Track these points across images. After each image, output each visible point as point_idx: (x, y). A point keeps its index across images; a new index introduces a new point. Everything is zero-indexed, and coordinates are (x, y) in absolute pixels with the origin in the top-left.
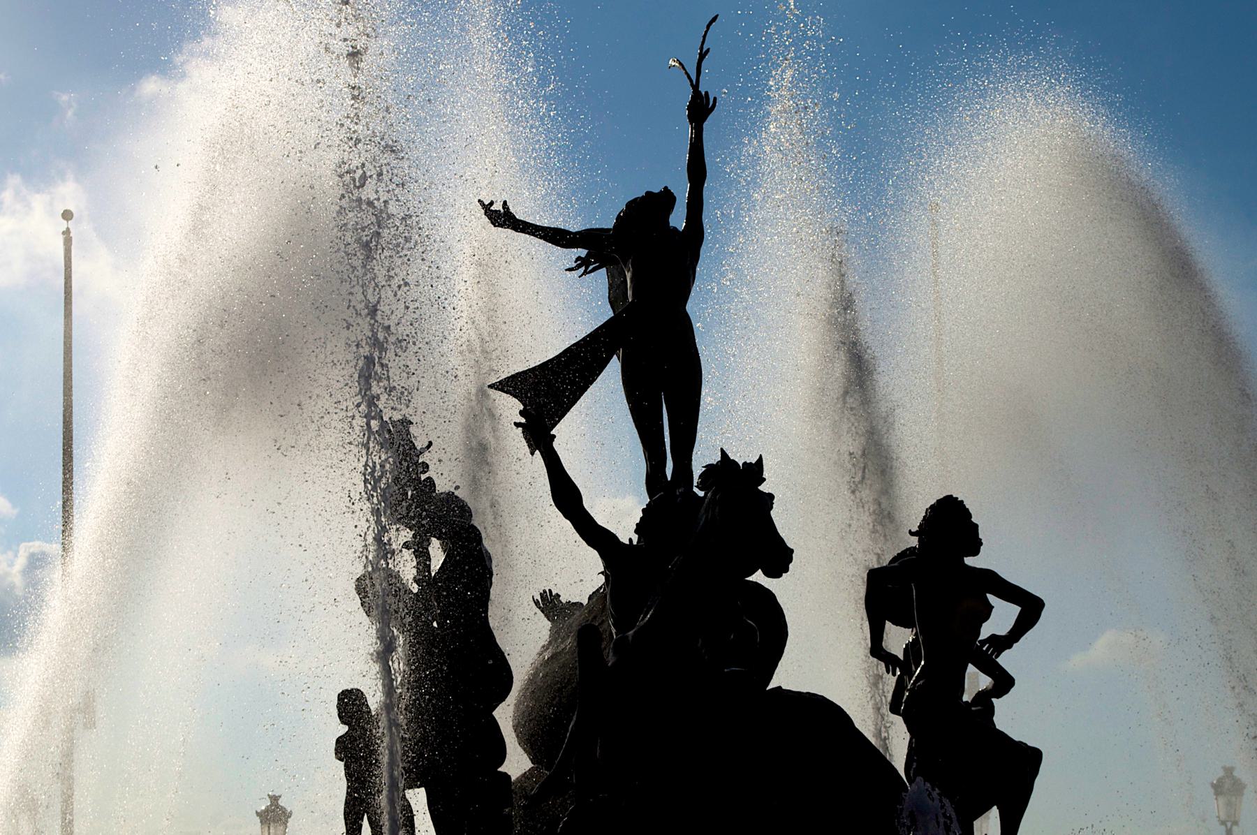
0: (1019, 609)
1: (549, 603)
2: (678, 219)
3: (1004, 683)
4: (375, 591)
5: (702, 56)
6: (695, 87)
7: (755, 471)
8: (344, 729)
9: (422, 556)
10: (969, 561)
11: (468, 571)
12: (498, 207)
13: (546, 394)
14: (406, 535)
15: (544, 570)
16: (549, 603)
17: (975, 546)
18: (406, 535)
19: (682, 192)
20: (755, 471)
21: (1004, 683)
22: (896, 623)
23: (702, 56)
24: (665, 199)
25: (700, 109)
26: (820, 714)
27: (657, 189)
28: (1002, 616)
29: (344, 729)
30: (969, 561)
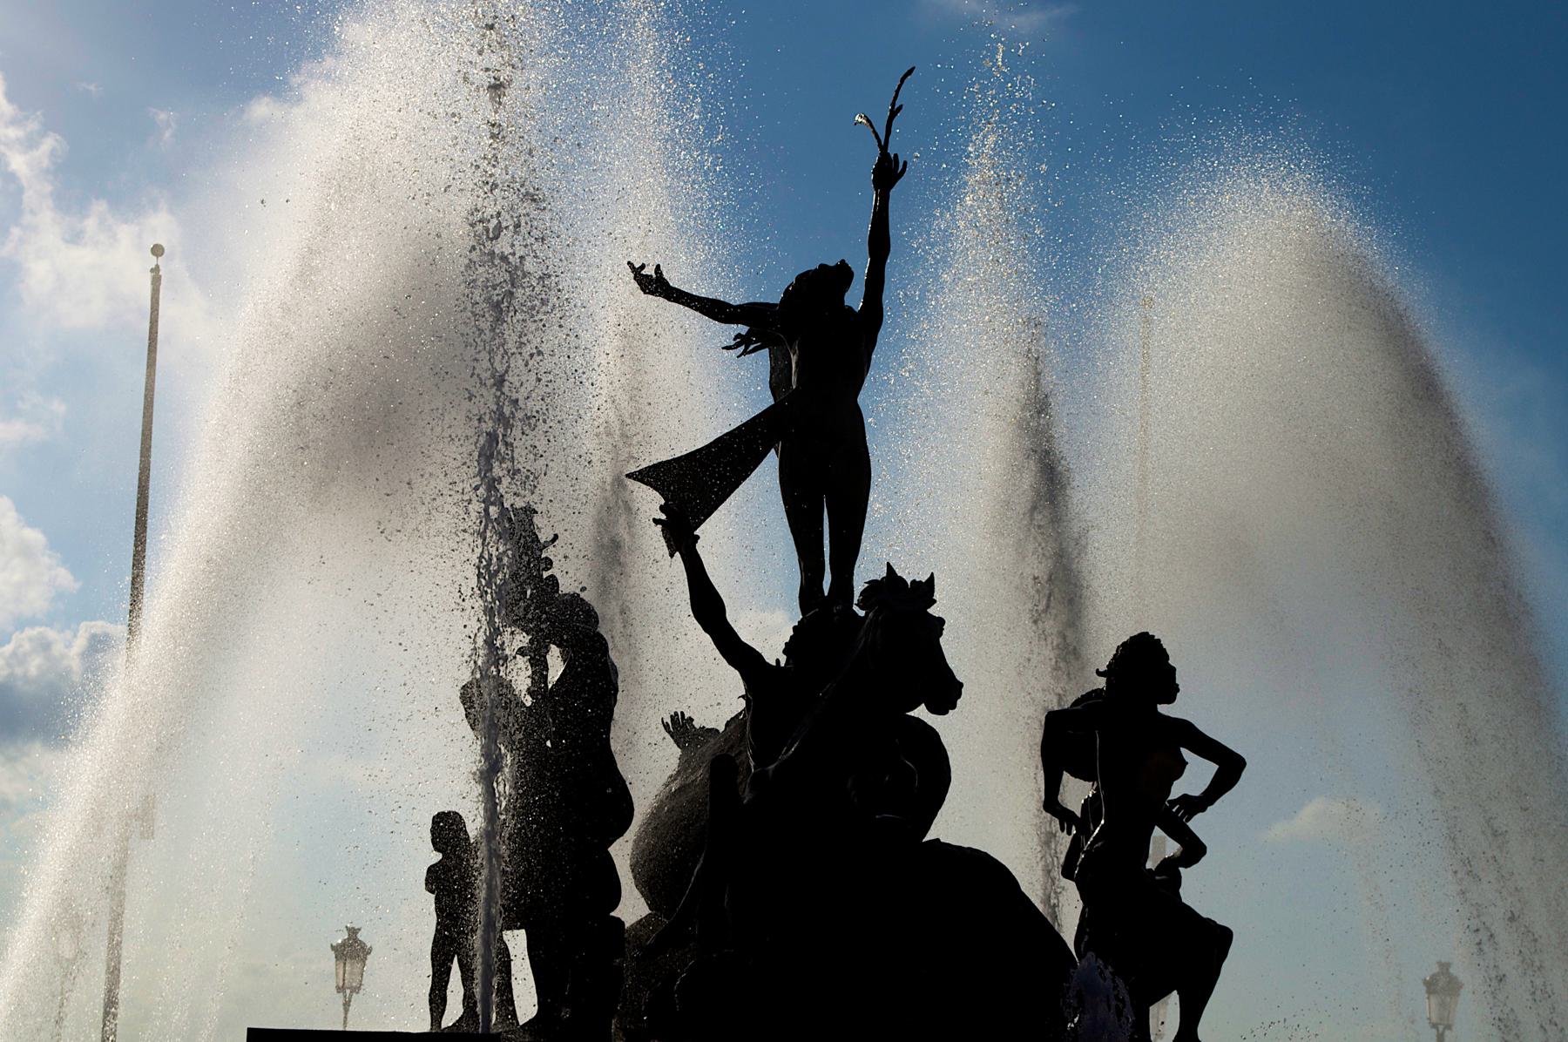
0: (1215, 767)
2: (854, 298)
3: (1193, 850)
4: (483, 702)
5: (894, 113)
6: (883, 148)
8: (437, 857)
10: (1163, 709)
11: (591, 686)
12: (649, 271)
13: (691, 488)
15: (674, 687)
18: (522, 639)
19: (861, 267)
21: (1193, 850)
23: (894, 113)
24: (843, 273)
25: (887, 173)
27: (832, 262)
28: (1197, 774)
29: (437, 857)
30: (1163, 709)
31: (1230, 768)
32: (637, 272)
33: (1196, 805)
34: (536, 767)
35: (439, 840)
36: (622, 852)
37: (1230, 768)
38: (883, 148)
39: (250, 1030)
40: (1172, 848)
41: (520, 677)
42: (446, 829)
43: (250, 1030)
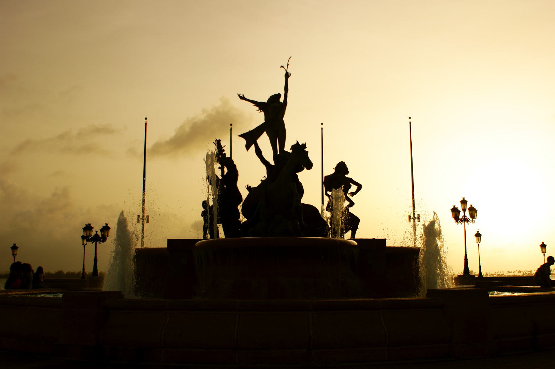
0: (166, 246)
1: (249, 188)
2: (282, 100)
3: (352, 204)
4: (211, 179)
5: (288, 65)
6: (286, 71)
7: (304, 146)
8: (204, 210)
9: (223, 171)
10: (346, 176)
11: (232, 173)
12: (241, 95)
13: (251, 138)
14: (220, 165)
15: (251, 173)
16: (249, 188)
17: (347, 173)
18: (220, 165)
19: (283, 94)
20: (304, 146)
21: (352, 204)
22: (193, 242)
23: (288, 65)
24: (279, 96)
25: (287, 75)
26: (311, 209)
27: (277, 93)
28: (354, 188)
29: (204, 210)
30: (346, 176)
31: (360, 187)
32: (239, 95)
33: (353, 194)
34: (222, 190)
35: (204, 207)
36: (240, 208)
37: (360, 187)
38: (286, 71)
39: (168, 240)
40: (347, 203)
41: (218, 173)
42: (205, 204)
43: (168, 240)
